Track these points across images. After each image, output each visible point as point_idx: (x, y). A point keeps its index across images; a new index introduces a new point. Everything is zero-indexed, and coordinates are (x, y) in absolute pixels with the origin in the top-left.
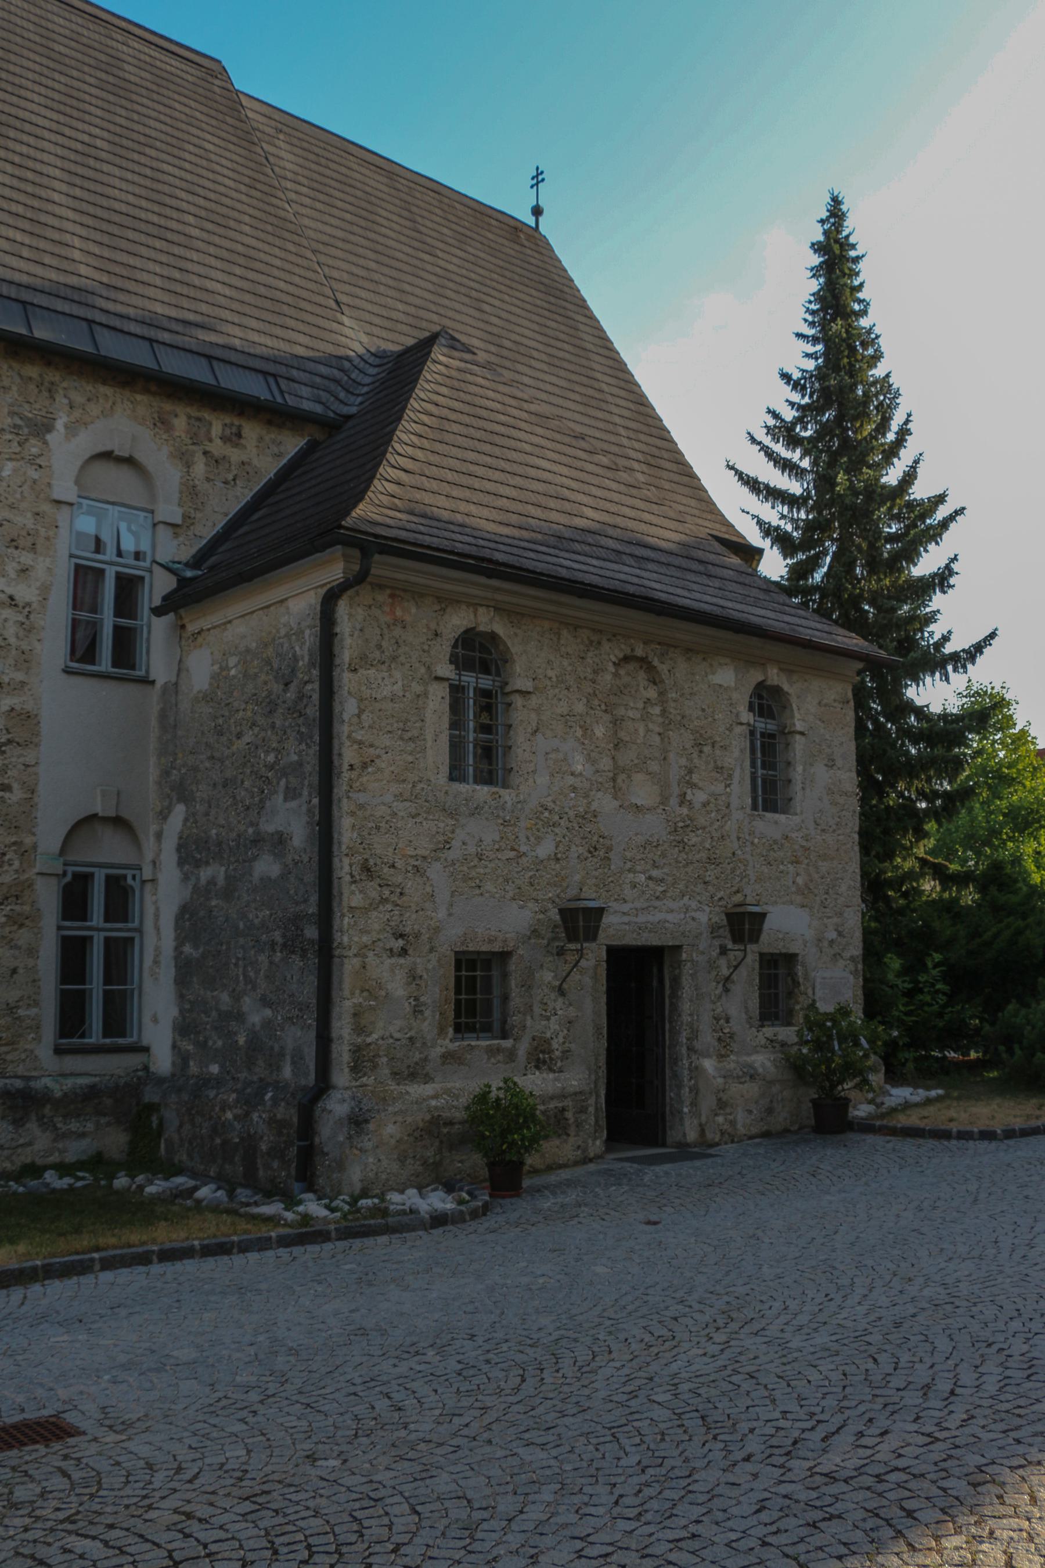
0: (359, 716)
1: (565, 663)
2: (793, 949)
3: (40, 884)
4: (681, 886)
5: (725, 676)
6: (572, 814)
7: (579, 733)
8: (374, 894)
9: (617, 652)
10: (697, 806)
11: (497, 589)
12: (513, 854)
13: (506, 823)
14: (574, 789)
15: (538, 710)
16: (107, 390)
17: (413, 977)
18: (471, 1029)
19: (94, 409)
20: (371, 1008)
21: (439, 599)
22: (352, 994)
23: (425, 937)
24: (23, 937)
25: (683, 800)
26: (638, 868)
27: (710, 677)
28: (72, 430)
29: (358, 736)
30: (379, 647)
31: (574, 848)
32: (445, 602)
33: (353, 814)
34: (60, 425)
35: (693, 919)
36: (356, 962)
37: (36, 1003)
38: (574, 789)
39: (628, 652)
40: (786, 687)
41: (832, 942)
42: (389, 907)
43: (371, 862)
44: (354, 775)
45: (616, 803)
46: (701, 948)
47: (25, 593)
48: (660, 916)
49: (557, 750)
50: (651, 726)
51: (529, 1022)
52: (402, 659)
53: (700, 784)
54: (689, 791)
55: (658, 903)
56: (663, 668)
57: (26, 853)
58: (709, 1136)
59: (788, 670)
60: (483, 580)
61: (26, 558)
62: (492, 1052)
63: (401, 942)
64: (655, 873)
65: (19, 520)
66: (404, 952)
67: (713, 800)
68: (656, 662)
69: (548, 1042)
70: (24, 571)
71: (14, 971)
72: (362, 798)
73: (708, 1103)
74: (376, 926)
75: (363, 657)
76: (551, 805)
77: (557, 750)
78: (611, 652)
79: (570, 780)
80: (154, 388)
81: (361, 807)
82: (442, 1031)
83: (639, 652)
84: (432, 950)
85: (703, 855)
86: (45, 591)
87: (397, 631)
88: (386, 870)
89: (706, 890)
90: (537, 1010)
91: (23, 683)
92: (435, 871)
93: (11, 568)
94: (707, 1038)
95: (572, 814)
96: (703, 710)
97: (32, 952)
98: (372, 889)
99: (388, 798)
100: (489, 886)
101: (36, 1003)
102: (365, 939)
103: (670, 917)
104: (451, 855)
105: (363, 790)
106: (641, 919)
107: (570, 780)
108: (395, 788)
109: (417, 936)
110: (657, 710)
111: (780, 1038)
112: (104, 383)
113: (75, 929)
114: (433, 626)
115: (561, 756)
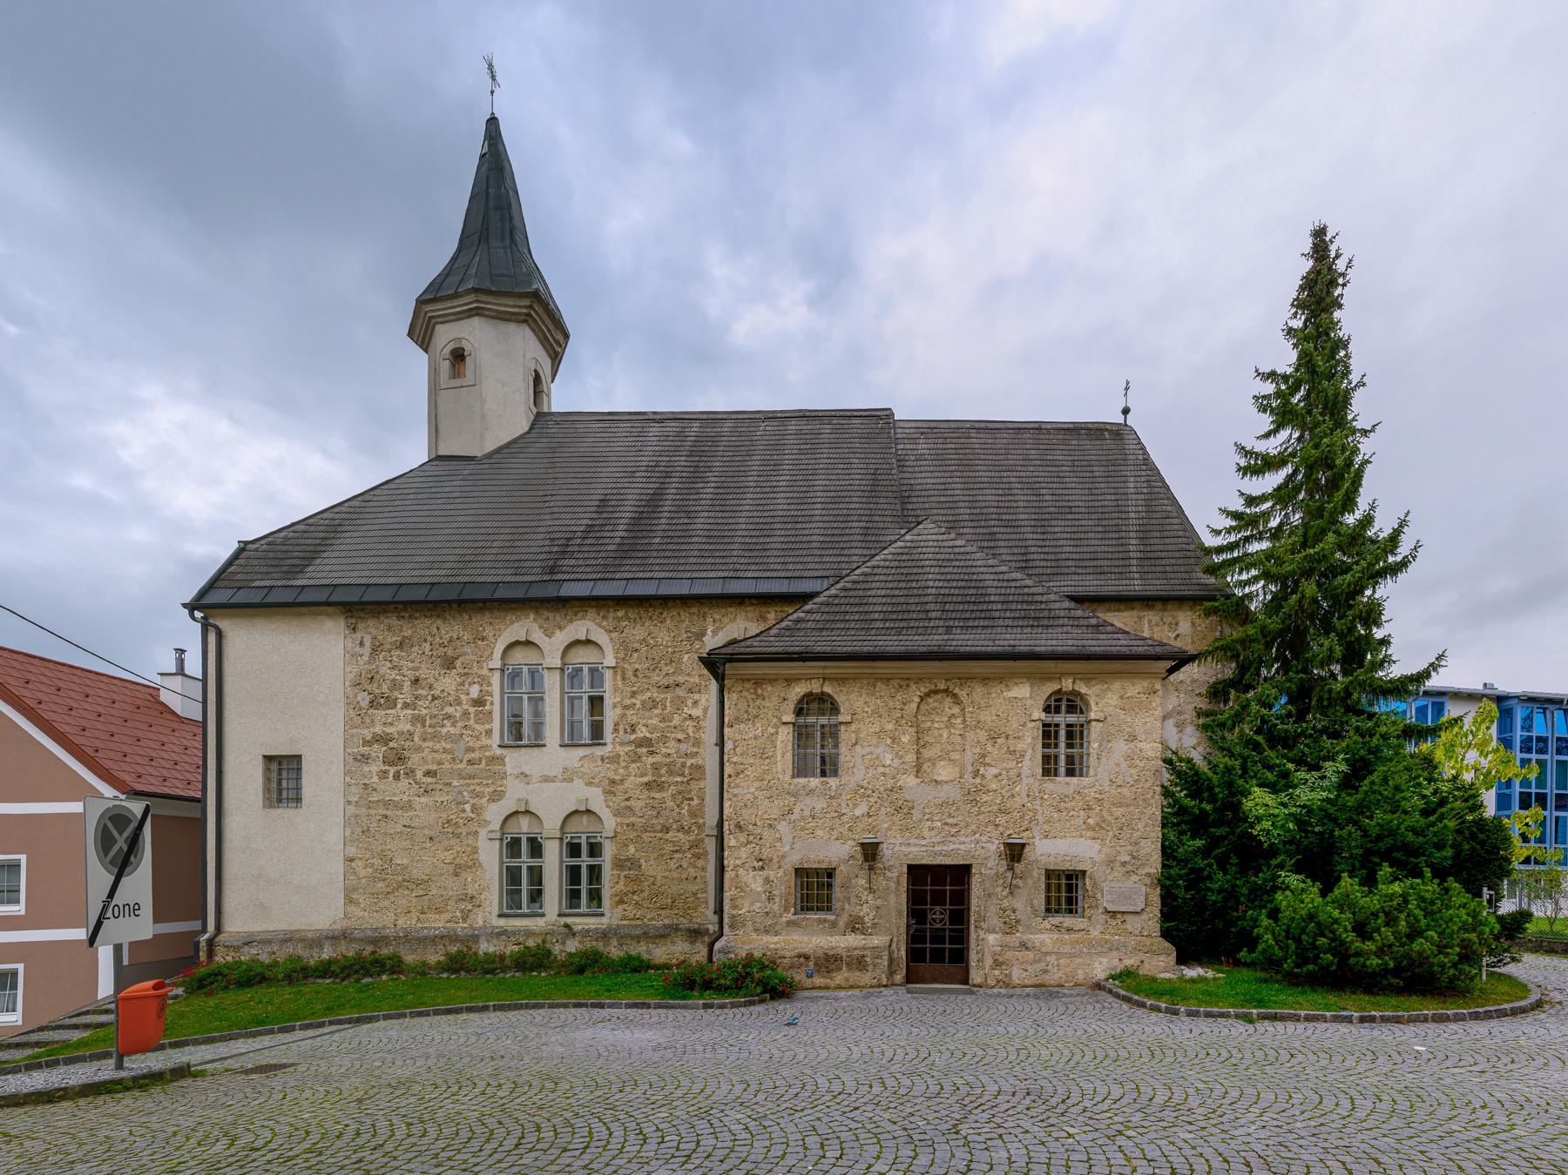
0: (734, 749)
1: (879, 702)
2: (1081, 867)
3: (707, 840)
4: (973, 827)
5: (1022, 691)
6: (882, 789)
7: (889, 741)
8: (742, 839)
9: (922, 689)
10: (989, 777)
11: (824, 667)
12: (836, 814)
13: (831, 798)
14: (884, 775)
15: (857, 732)
16: (732, 609)
17: (767, 881)
18: (810, 909)
19: (726, 620)
20: (741, 896)
21: (787, 680)
22: (730, 889)
23: (775, 860)
24: (700, 863)
25: (976, 774)
26: (935, 818)
27: (1005, 694)
28: (715, 633)
29: (734, 760)
30: (747, 712)
31: (883, 809)
32: (790, 681)
33: (730, 799)
34: (709, 632)
35: (983, 848)
36: (733, 874)
37: (706, 892)
38: (884, 775)
39: (933, 687)
40: (1083, 690)
41: (1124, 864)
42: (753, 845)
43: (742, 823)
44: (731, 780)
45: (919, 780)
46: (989, 866)
47: (697, 712)
48: (952, 847)
49: (871, 753)
50: (953, 731)
51: (847, 907)
52: (762, 716)
53: (993, 763)
54: (982, 769)
55: (952, 839)
56: (962, 694)
57: (700, 827)
58: (989, 982)
59: (1076, 676)
60: (801, 663)
61: (696, 696)
62: (820, 921)
63: (761, 863)
64: (950, 821)
65: (692, 680)
66: (762, 868)
67: (1004, 772)
68: (957, 690)
69: (862, 918)
70: (696, 703)
71: (696, 878)
72: (736, 791)
73: (989, 962)
74: (744, 856)
75: (737, 719)
76: (865, 785)
77: (871, 753)
78: (915, 692)
79: (881, 770)
80: (755, 602)
81: (735, 796)
82: (786, 910)
83: (942, 686)
84: (779, 867)
85: (995, 808)
86: (706, 710)
87: (759, 702)
88: (751, 827)
89: (996, 830)
90: (853, 900)
91: (697, 753)
92: (783, 827)
93: (689, 703)
94: (994, 921)
95: (882, 789)
96: (998, 716)
97: (703, 869)
98: (743, 838)
99: (752, 790)
100: (820, 833)
101: (706, 892)
102: (738, 862)
103: (962, 847)
104: (793, 817)
105: (737, 786)
106: (937, 848)
107: (881, 770)
108: (756, 784)
109: (771, 860)
110: (959, 721)
111: (1065, 925)
112: (731, 606)
113: (514, 863)
114: (782, 695)
115: (874, 756)
